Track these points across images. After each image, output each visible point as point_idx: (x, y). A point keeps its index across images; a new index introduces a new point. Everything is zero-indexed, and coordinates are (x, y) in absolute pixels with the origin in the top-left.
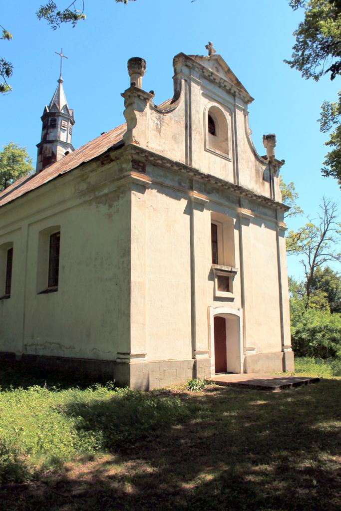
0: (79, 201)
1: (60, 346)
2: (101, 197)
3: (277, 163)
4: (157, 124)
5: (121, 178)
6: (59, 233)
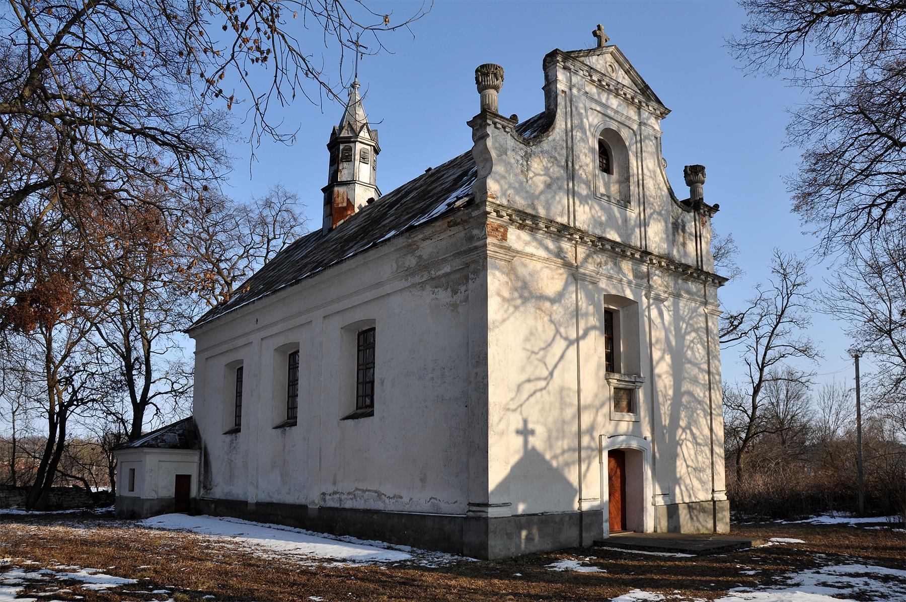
1: (379, 495)
2: (439, 277)
5: (471, 250)
6: (374, 329)
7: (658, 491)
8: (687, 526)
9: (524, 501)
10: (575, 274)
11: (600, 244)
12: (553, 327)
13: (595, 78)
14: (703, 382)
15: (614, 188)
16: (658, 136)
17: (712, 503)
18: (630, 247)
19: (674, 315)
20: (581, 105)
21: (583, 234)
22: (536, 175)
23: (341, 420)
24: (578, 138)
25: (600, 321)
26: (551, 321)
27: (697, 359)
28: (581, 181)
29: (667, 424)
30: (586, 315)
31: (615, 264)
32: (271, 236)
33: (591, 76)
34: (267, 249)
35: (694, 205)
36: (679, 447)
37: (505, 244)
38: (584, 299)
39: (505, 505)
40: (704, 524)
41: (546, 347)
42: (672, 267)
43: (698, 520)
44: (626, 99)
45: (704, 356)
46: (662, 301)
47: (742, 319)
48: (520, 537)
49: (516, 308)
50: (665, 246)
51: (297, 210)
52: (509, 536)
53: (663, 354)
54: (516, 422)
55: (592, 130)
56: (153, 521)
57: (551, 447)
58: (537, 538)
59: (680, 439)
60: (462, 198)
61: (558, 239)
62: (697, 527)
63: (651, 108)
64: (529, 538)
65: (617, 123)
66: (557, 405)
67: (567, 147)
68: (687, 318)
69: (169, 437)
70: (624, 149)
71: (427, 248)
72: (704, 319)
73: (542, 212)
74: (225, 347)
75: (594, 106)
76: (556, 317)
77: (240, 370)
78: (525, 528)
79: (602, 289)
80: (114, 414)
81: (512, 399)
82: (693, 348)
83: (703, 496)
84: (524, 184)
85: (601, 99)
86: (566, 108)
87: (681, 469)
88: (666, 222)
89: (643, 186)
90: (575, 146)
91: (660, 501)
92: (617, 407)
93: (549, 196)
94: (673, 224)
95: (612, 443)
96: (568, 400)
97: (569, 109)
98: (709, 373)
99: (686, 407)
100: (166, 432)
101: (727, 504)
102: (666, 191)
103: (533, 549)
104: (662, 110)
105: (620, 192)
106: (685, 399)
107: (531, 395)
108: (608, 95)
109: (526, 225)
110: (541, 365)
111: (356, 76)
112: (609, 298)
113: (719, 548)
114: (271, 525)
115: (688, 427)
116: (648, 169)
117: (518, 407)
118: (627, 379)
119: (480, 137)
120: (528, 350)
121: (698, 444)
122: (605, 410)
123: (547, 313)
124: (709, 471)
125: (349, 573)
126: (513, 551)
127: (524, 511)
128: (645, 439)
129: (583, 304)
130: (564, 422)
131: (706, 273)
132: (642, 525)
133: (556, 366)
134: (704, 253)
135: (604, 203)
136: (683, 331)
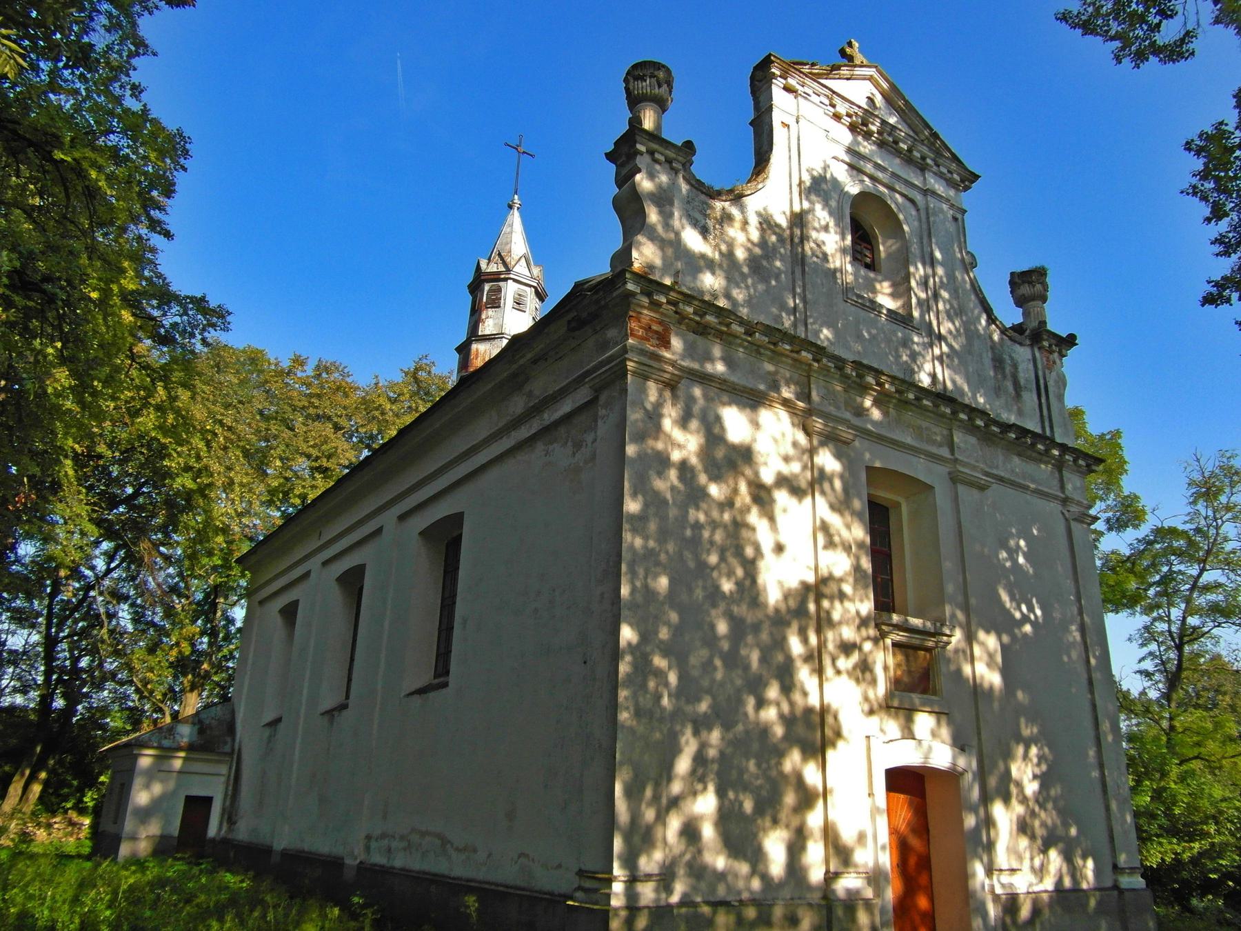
1: (445, 841)
3: (1053, 341)
94: (994, 360)
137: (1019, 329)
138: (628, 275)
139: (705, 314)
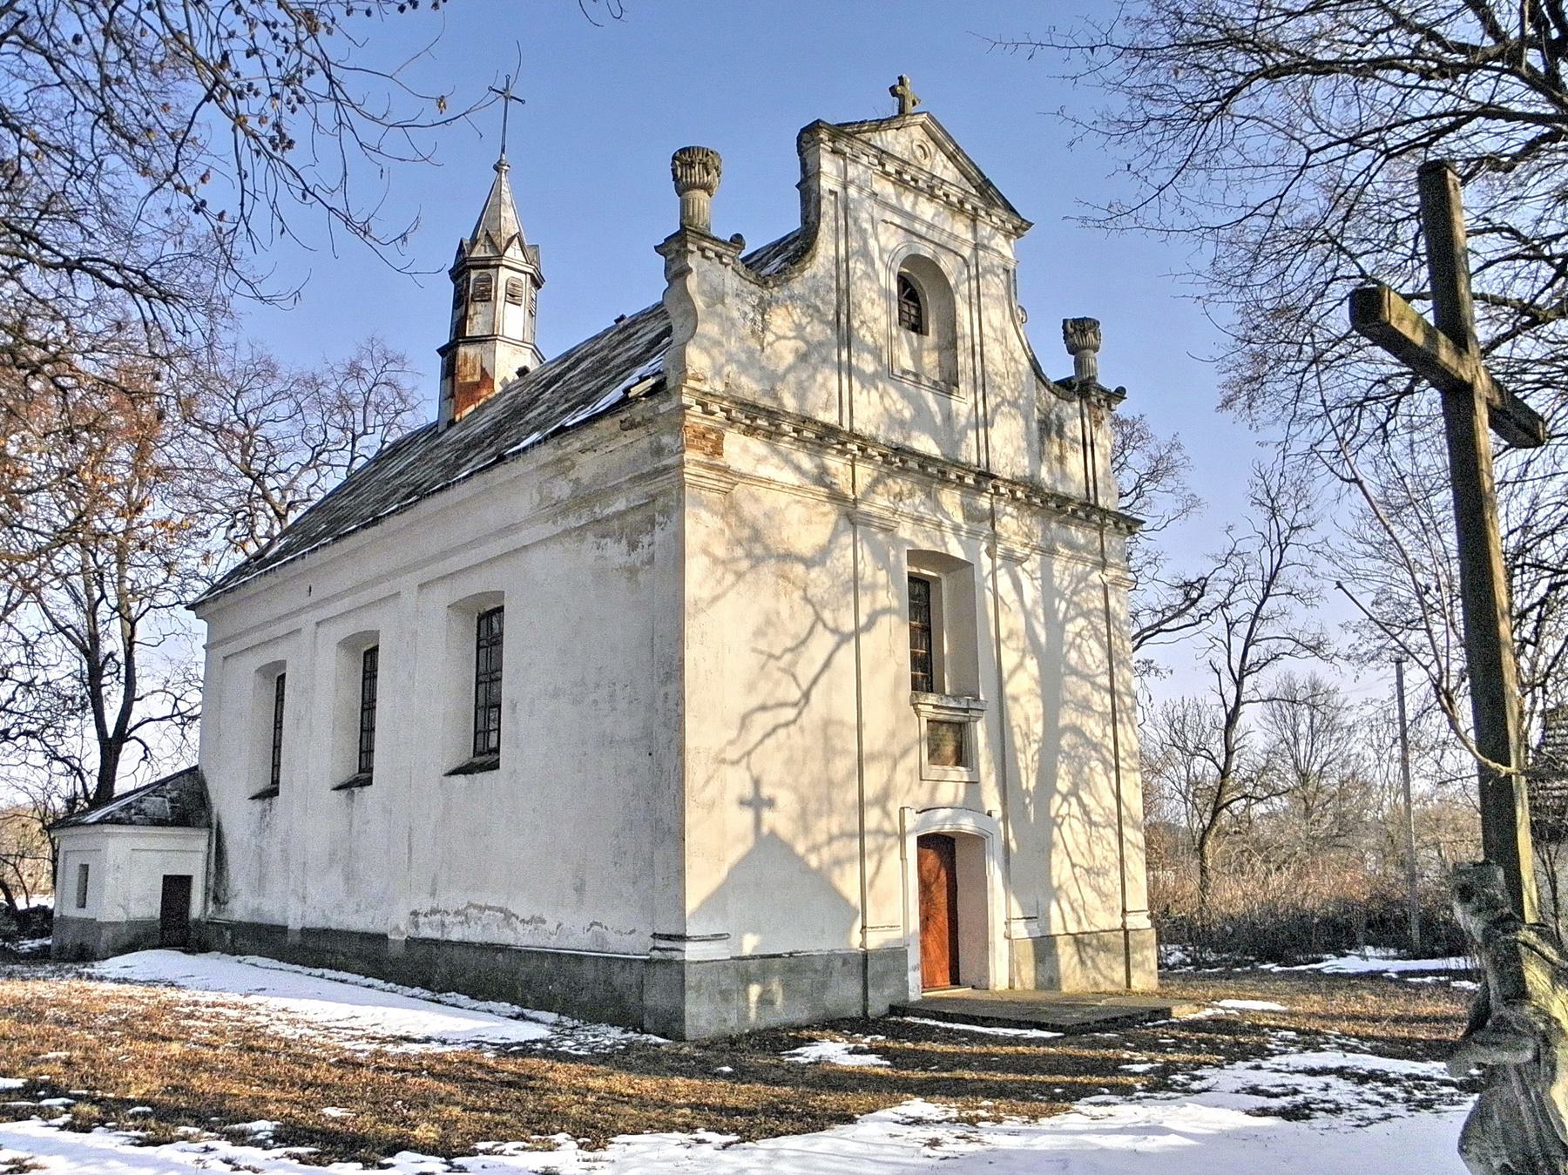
0: (547, 530)
1: (508, 916)
2: (608, 519)
4: (753, 320)
5: (658, 472)
6: (501, 610)
7: (1017, 912)
8: (1074, 977)
9: (755, 930)
10: (850, 513)
11: (899, 459)
12: (809, 609)
13: (890, 168)
14: (1100, 709)
15: (930, 360)
16: (1011, 266)
17: (1122, 933)
18: (956, 463)
19: (1042, 586)
20: (864, 215)
21: (865, 442)
22: (779, 338)
23: (445, 775)
24: (859, 273)
25: (898, 597)
26: (807, 599)
27: (1088, 667)
28: (864, 347)
29: (1031, 789)
30: (873, 587)
31: (928, 495)
32: (359, 429)
33: (883, 165)
34: (352, 452)
35: (1079, 387)
36: (1056, 830)
37: (718, 461)
38: (868, 558)
39: (717, 937)
40: (1107, 972)
41: (797, 646)
42: (1037, 501)
43: (1096, 967)
44: (948, 204)
45: (1102, 662)
46: (1020, 561)
47: (1203, 587)
48: (747, 999)
49: (740, 576)
50: (1026, 462)
51: (406, 383)
52: (725, 995)
53: (1023, 656)
54: (737, 782)
55: (886, 257)
56: (113, 966)
57: (806, 830)
58: (779, 1000)
59: (1057, 816)
60: (648, 377)
61: (818, 452)
62: (1094, 979)
63: (995, 219)
64: (765, 1001)
65: (932, 246)
66: (819, 753)
67: (838, 289)
68: (1068, 592)
69: (153, 805)
70: (947, 292)
71: (588, 467)
72: (1101, 594)
73: (790, 404)
74: (256, 638)
75: (889, 216)
76: (815, 592)
77: (281, 679)
78: (758, 981)
79: (904, 541)
80: (63, 760)
81: (731, 743)
82: (1080, 646)
83: (1106, 920)
84: (757, 355)
85: (902, 204)
86: (837, 222)
87: (1060, 870)
88: (1026, 419)
89: (982, 355)
90: (853, 287)
91: (1020, 930)
92: (935, 755)
93: (804, 376)
95: (925, 822)
96: (838, 743)
97: (842, 222)
98: (1112, 692)
99: (1068, 756)
100: (147, 795)
101: (1151, 935)
102: (1027, 364)
103: (772, 1021)
104: (1017, 222)
105: (940, 366)
106: (1066, 741)
107: (768, 735)
108: (916, 197)
109: (757, 428)
110: (787, 679)
111: (503, 151)
112: (916, 556)
113: (1106, 1021)
114: (326, 971)
115: (1074, 792)
116: (991, 326)
117: (742, 757)
118: (953, 704)
119: (677, 275)
120: (762, 652)
121: (1092, 823)
122: (911, 761)
123: (799, 584)
124: (1115, 875)
125: (420, 1064)
126: (733, 1025)
127: (755, 948)
128: (989, 814)
129: (867, 568)
130: (831, 783)
131: (1102, 510)
132: (987, 977)
133: (815, 681)
134: (1099, 474)
135: (908, 385)
136: (1061, 616)
137: (1065, 384)
138: (684, 390)
139: (756, 418)
